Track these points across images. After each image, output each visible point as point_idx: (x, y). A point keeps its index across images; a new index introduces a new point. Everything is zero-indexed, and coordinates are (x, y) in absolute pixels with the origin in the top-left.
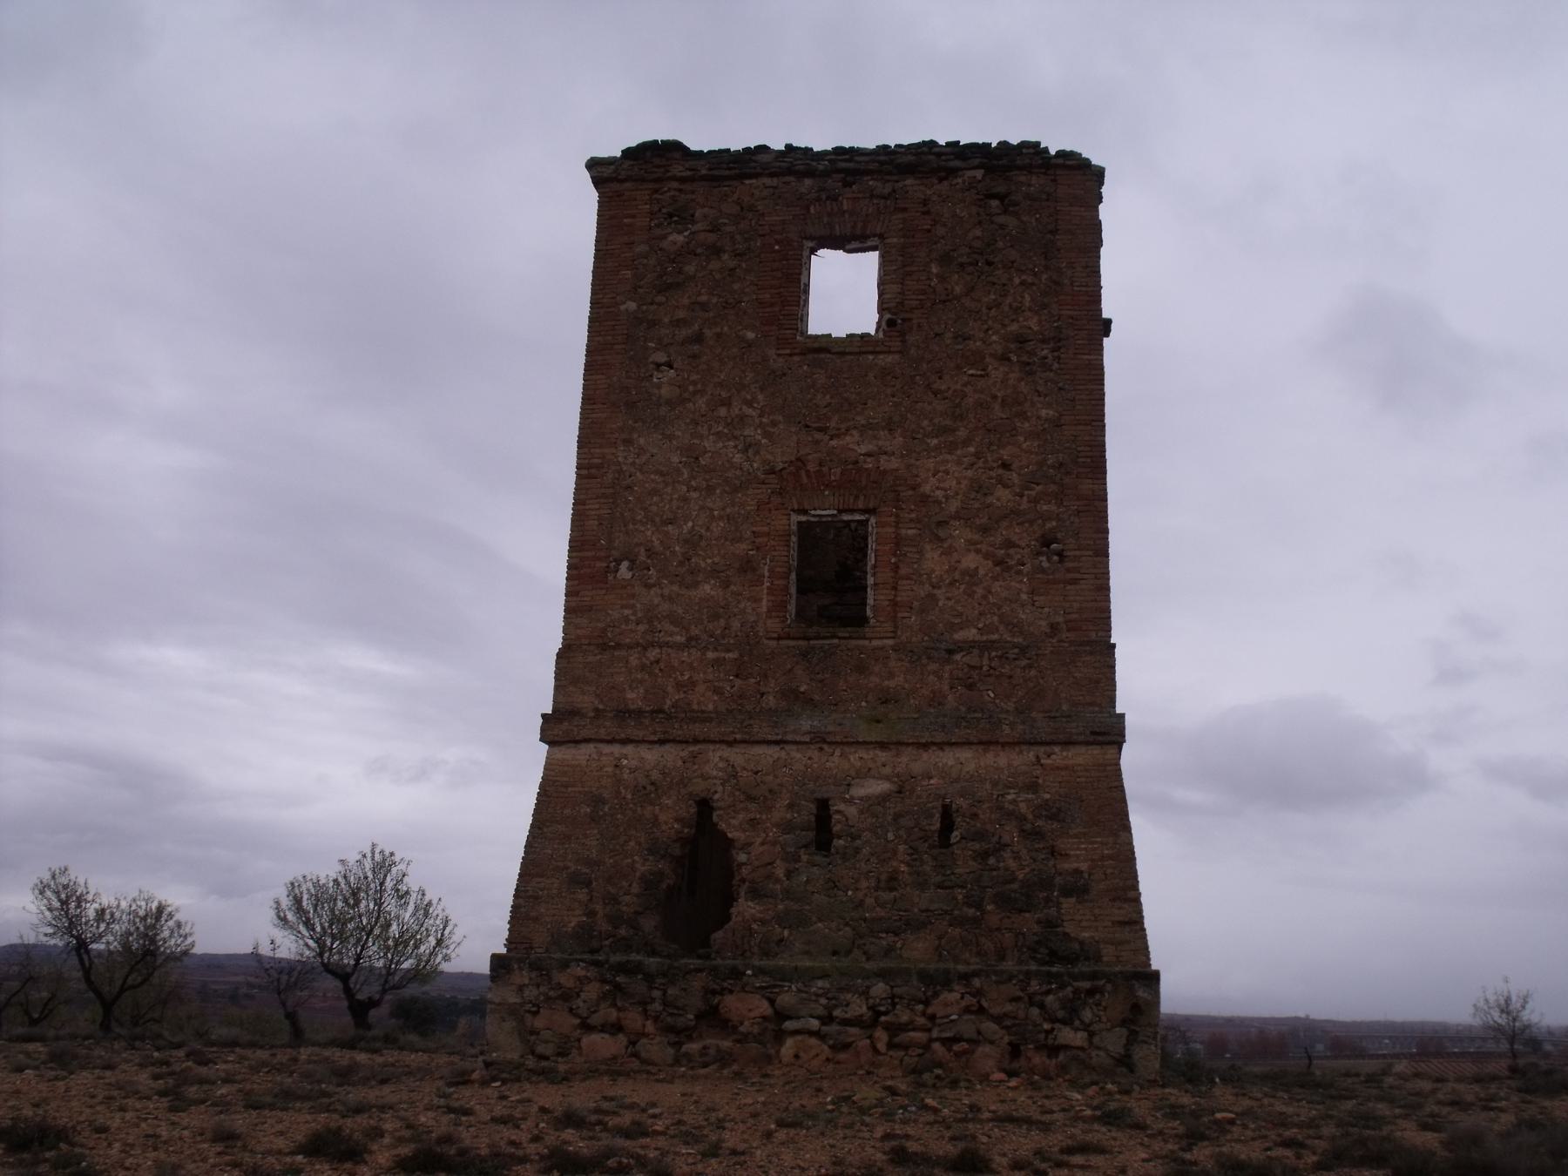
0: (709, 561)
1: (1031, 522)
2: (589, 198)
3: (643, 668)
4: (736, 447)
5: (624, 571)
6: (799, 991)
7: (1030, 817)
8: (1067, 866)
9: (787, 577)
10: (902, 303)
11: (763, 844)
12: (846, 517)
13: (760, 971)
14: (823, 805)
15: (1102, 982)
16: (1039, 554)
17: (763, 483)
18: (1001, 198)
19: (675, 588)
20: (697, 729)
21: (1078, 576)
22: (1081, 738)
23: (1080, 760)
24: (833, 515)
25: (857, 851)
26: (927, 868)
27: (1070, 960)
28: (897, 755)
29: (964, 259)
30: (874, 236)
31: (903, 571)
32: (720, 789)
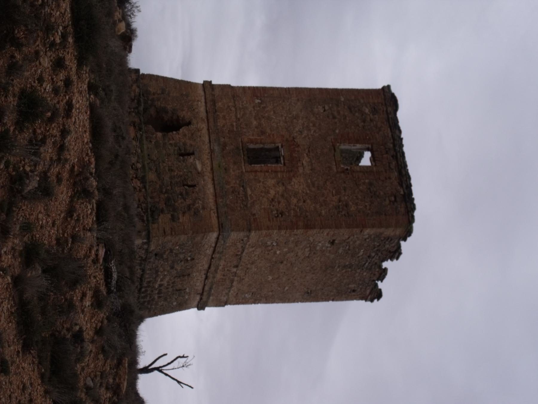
0: (263, 123)
1: (287, 208)
2: (379, 86)
3: (229, 107)
4: (300, 128)
5: (257, 101)
6: (137, 145)
7: (194, 207)
8: (180, 216)
9: (261, 143)
10: (354, 172)
11: (179, 137)
12: (282, 158)
13: (142, 135)
14: (193, 154)
15: (146, 222)
16: (277, 211)
17: (290, 136)
18: (395, 201)
19: (254, 114)
20: (211, 120)
21: (271, 221)
22: (220, 220)
23: (213, 221)
24: (282, 154)
25: (180, 162)
26: (176, 179)
27: (152, 216)
28: (210, 173)
29: (372, 189)
30: (376, 164)
31: (267, 174)
32: (194, 127)
